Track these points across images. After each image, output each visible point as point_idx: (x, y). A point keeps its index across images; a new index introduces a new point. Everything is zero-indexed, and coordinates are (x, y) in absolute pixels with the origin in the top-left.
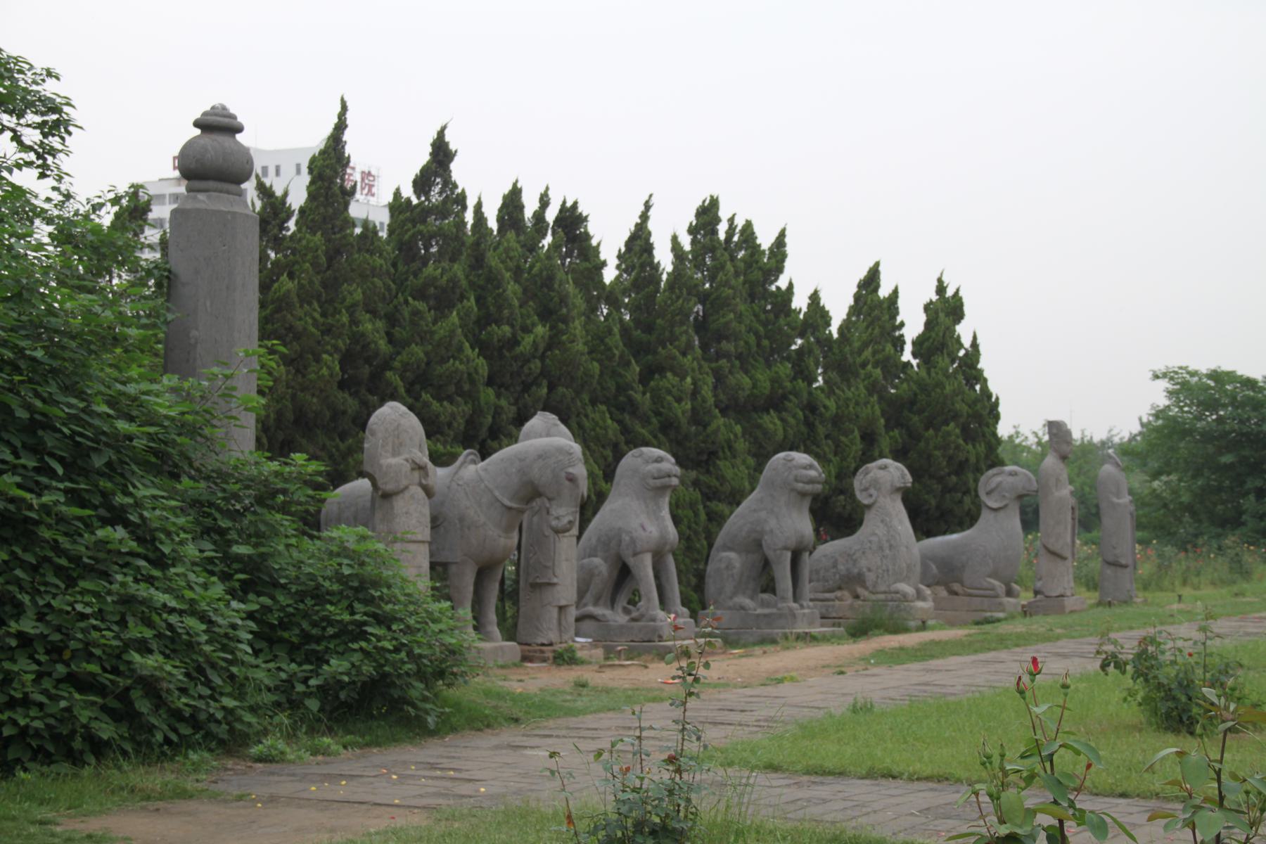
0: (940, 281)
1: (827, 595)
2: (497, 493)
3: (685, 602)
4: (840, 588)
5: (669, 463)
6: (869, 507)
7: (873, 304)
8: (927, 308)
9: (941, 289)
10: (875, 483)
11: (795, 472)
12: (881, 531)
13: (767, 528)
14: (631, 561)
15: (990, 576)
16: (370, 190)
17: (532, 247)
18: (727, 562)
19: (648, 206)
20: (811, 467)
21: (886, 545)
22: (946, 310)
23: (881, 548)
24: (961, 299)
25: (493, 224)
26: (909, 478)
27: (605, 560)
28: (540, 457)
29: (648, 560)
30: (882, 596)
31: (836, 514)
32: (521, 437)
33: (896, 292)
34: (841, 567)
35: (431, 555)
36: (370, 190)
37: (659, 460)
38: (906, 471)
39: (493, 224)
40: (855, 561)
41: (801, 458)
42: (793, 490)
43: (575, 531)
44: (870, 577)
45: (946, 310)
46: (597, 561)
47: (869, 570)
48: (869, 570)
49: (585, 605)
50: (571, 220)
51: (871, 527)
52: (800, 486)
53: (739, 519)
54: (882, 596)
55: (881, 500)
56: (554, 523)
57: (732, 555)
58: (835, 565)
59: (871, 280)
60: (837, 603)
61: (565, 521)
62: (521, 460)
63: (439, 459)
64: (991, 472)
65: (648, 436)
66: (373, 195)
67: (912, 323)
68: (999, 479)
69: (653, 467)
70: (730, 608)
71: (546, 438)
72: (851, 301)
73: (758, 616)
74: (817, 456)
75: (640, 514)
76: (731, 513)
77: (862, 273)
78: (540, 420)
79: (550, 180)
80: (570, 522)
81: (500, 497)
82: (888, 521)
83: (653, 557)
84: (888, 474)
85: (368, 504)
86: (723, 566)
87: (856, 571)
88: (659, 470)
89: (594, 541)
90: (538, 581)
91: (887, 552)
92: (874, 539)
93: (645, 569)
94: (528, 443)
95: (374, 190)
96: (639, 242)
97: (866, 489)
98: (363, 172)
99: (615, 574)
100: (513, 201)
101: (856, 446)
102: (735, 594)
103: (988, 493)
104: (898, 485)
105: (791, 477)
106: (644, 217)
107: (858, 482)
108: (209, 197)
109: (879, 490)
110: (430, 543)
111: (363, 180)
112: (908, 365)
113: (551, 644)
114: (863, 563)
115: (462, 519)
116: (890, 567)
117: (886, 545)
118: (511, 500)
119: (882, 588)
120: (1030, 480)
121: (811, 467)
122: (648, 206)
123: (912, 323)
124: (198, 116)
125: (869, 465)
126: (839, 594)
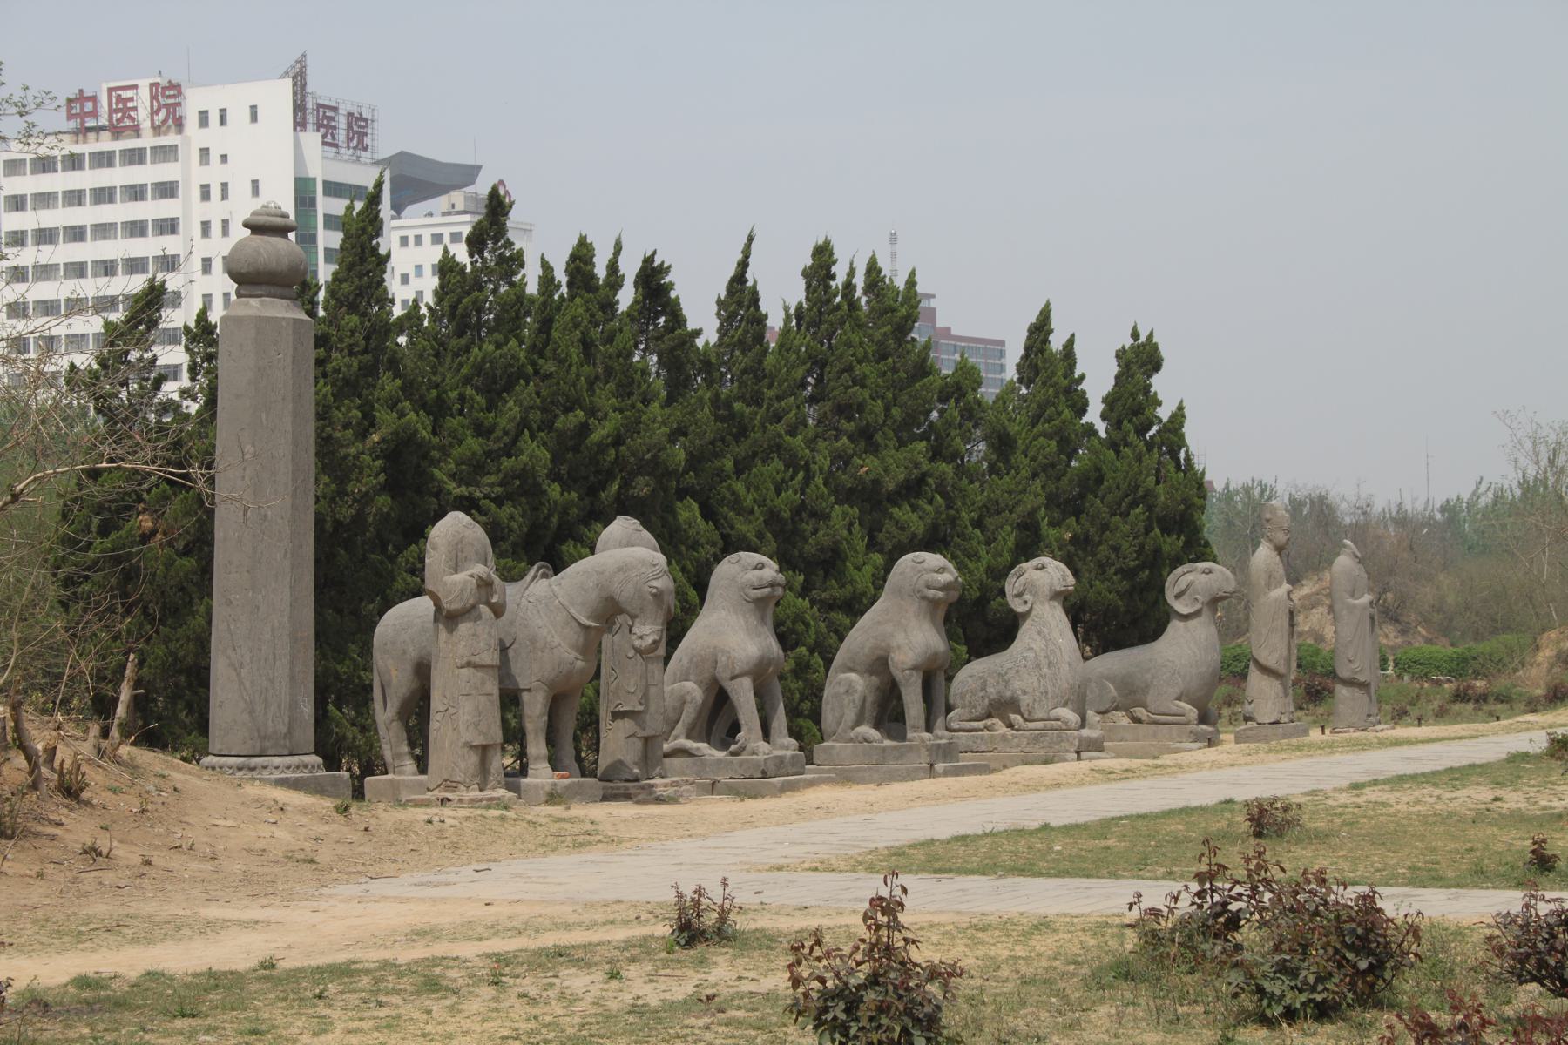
0: (1135, 328)
1: (975, 724)
2: (573, 611)
3: (794, 733)
4: (989, 716)
5: (771, 570)
6: (1026, 615)
7: (1046, 362)
8: (1121, 354)
9: (1135, 335)
10: (1029, 587)
11: (926, 576)
12: (1038, 645)
13: (894, 644)
14: (729, 686)
15: (1179, 699)
16: (361, 141)
17: (609, 306)
18: (846, 687)
19: (751, 239)
20: (942, 570)
21: (1044, 662)
22: (1141, 360)
23: (1038, 666)
24: (1155, 347)
25: (561, 276)
26: (1071, 580)
27: (699, 683)
28: (620, 569)
29: (746, 683)
30: (1040, 725)
31: (981, 624)
32: (599, 545)
33: (1071, 341)
34: (991, 690)
35: (501, 682)
36: (361, 141)
37: (760, 567)
38: (1068, 572)
39: (561, 276)
40: (1007, 682)
41: (933, 559)
42: (924, 598)
43: (661, 651)
44: (1025, 701)
45: (1141, 360)
46: (690, 685)
47: (1025, 693)
48: (1025, 693)
49: (676, 738)
50: (652, 279)
51: (1026, 636)
52: (931, 593)
53: (862, 636)
54: (1040, 725)
55: (1038, 609)
56: (637, 643)
57: (853, 676)
58: (983, 689)
59: (1040, 329)
60: (986, 733)
61: (650, 640)
62: (598, 573)
63: (510, 576)
64: (1180, 570)
65: (751, 536)
66: (365, 149)
67: (1098, 378)
68: (1190, 577)
69: (753, 576)
70: (851, 740)
71: (626, 552)
72: (1022, 352)
73: (884, 749)
74: (953, 558)
75: (730, 632)
76: (853, 625)
77: (1032, 317)
78: (622, 526)
79: (627, 234)
80: (655, 642)
81: (576, 615)
82: (1047, 635)
83: (754, 681)
84: (1042, 580)
85: (951, 654)
86: (842, 690)
87: (1009, 694)
88: (761, 579)
89: (685, 661)
90: (620, 708)
91: (1046, 670)
92: (1031, 655)
93: (743, 696)
94: (606, 554)
95: (367, 141)
96: (740, 298)
97: (1019, 595)
98: (350, 115)
99: (711, 699)
100: (581, 256)
101: (1008, 537)
102: (858, 723)
103: (1178, 597)
104: (1059, 588)
105: (921, 582)
106: (743, 265)
107: (1011, 585)
108: (262, 303)
109: (1035, 595)
110: (499, 668)
111: (349, 127)
112: (1090, 430)
113: (637, 780)
114: (1017, 684)
115: (533, 641)
116: (1050, 689)
117: (1044, 662)
118: (588, 618)
119: (1039, 714)
120: (1227, 579)
121: (942, 570)
122: (751, 239)
123: (1098, 378)
124: (248, 215)
125: (1024, 565)
126: (989, 722)
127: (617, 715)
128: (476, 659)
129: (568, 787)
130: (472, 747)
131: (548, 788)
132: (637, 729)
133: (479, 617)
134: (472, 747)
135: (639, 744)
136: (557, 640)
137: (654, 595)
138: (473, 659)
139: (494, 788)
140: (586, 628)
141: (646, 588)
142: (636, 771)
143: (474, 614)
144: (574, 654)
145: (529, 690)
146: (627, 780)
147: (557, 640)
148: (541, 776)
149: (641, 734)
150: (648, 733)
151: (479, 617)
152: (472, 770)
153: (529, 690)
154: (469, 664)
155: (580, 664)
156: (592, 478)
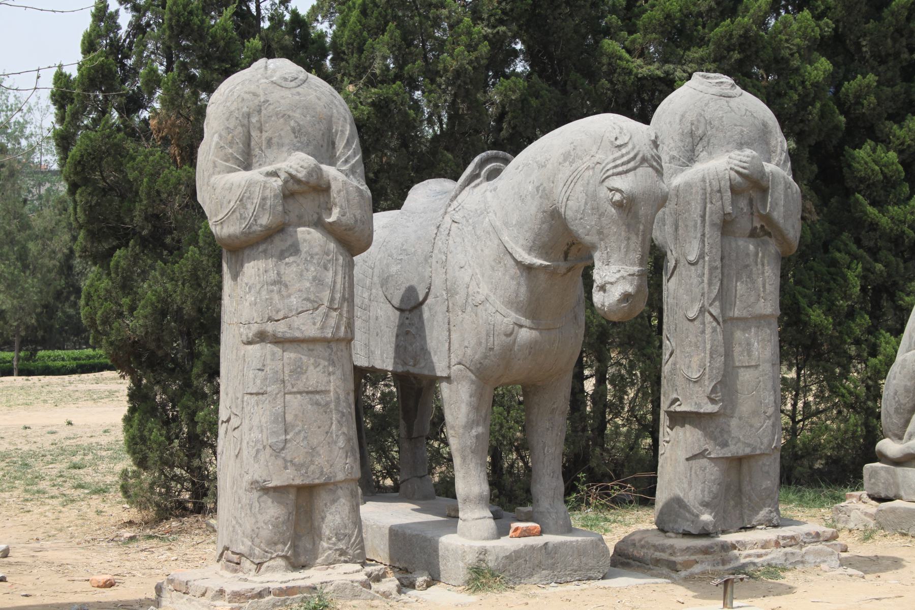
2: (505, 238)
81: (511, 245)
115: (451, 292)
118: (530, 250)
127: (678, 419)
128: (281, 328)
129: (514, 557)
130: (266, 490)
131: (471, 559)
132: (710, 446)
133: (294, 249)
134: (266, 490)
135: (713, 472)
136: (484, 290)
137: (619, 205)
138: (270, 327)
139: (330, 563)
140: (528, 269)
141: (604, 193)
142: (706, 517)
143: (279, 243)
144: (513, 316)
145: (448, 379)
146: (687, 534)
147: (484, 290)
148: (472, 534)
149: (716, 452)
150: (733, 450)
151: (294, 249)
152: (266, 532)
153: (448, 379)
154: (262, 337)
155: (525, 335)
156: (905, 56)
